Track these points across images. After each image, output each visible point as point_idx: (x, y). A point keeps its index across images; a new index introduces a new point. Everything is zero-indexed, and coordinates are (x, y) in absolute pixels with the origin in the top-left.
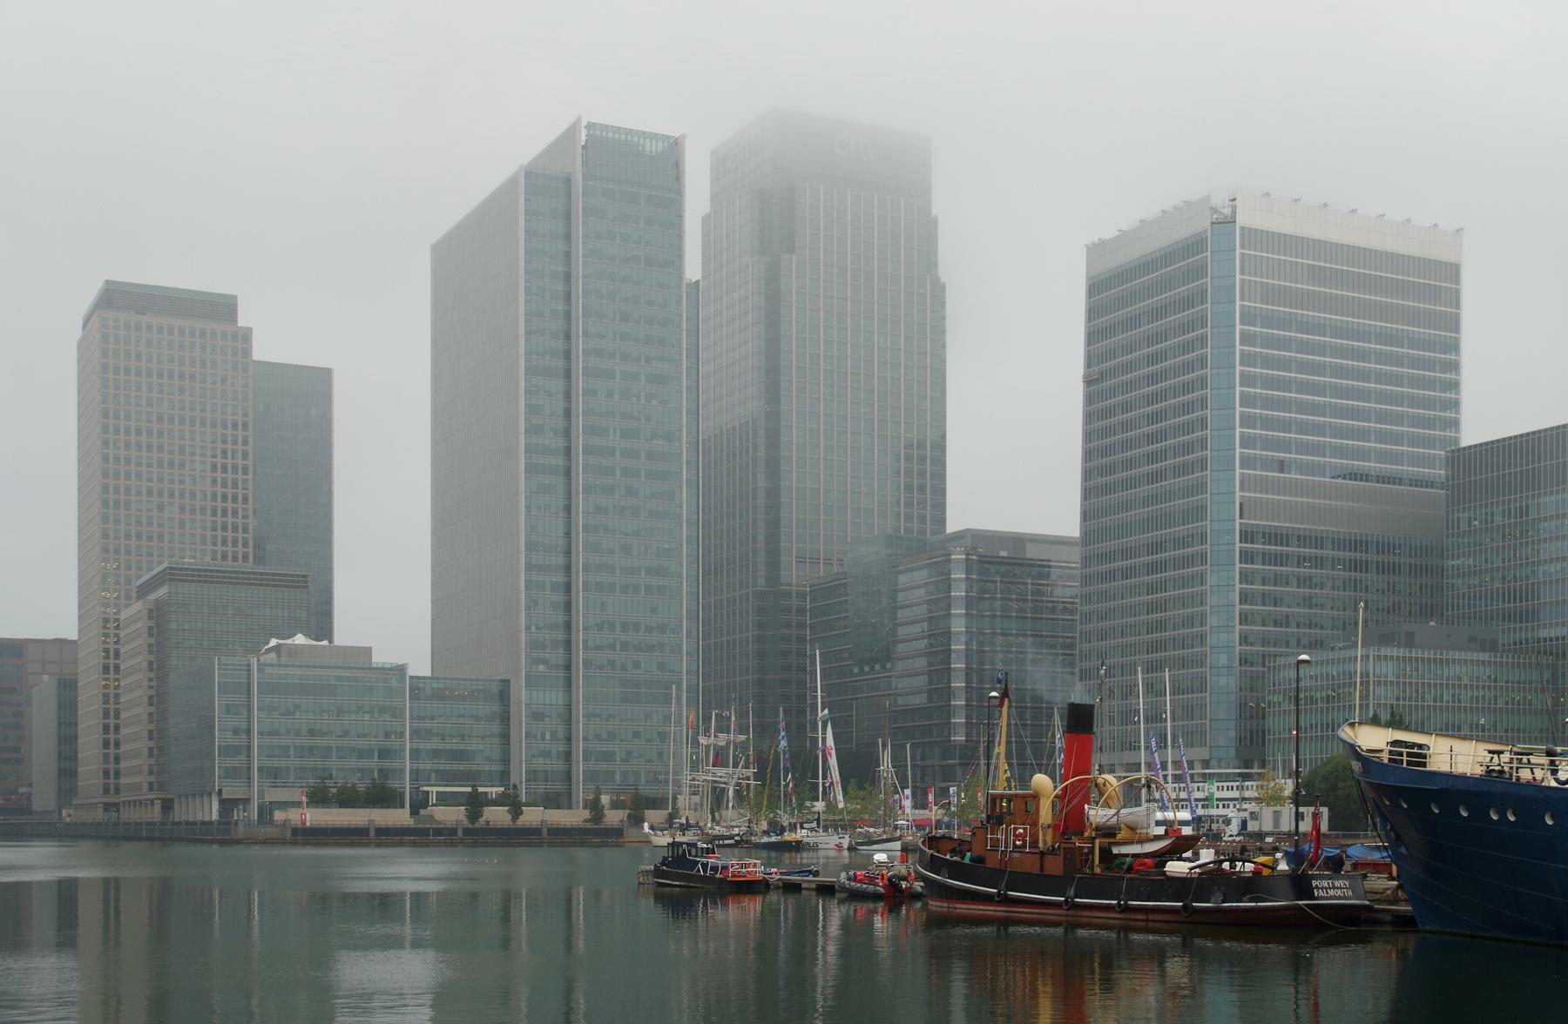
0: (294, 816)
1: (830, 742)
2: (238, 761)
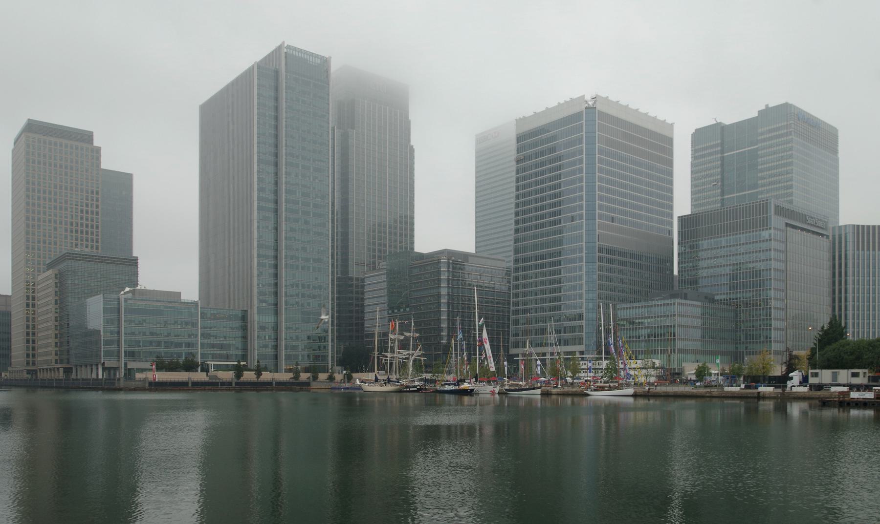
0: (150, 376)
1: (485, 335)
2: (114, 348)
